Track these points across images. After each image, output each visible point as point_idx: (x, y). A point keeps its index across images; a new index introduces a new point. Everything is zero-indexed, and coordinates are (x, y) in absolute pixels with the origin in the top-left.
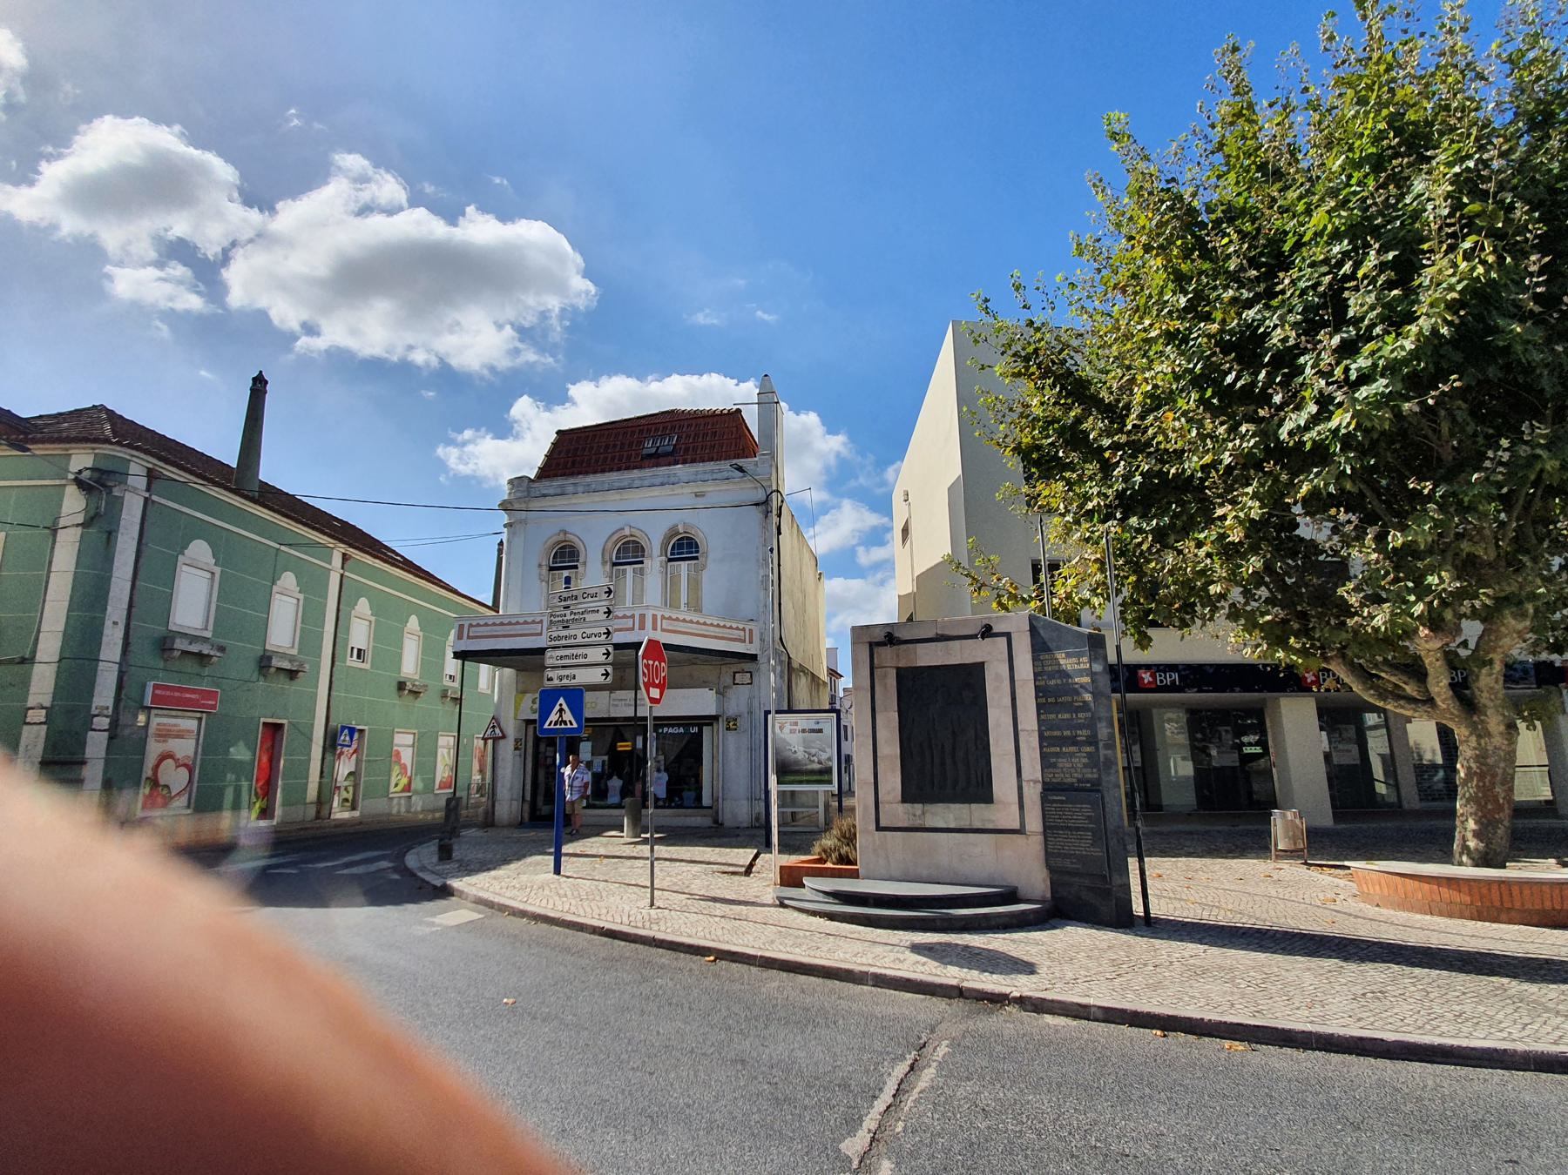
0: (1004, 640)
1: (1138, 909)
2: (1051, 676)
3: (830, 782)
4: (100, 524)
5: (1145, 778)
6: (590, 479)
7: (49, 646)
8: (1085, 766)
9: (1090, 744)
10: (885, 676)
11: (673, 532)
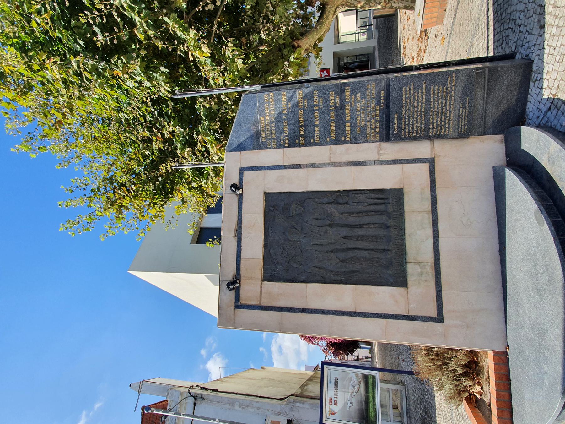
0: (246, 173)
2: (280, 131)
3: (374, 377)
8: (364, 96)
9: (343, 91)
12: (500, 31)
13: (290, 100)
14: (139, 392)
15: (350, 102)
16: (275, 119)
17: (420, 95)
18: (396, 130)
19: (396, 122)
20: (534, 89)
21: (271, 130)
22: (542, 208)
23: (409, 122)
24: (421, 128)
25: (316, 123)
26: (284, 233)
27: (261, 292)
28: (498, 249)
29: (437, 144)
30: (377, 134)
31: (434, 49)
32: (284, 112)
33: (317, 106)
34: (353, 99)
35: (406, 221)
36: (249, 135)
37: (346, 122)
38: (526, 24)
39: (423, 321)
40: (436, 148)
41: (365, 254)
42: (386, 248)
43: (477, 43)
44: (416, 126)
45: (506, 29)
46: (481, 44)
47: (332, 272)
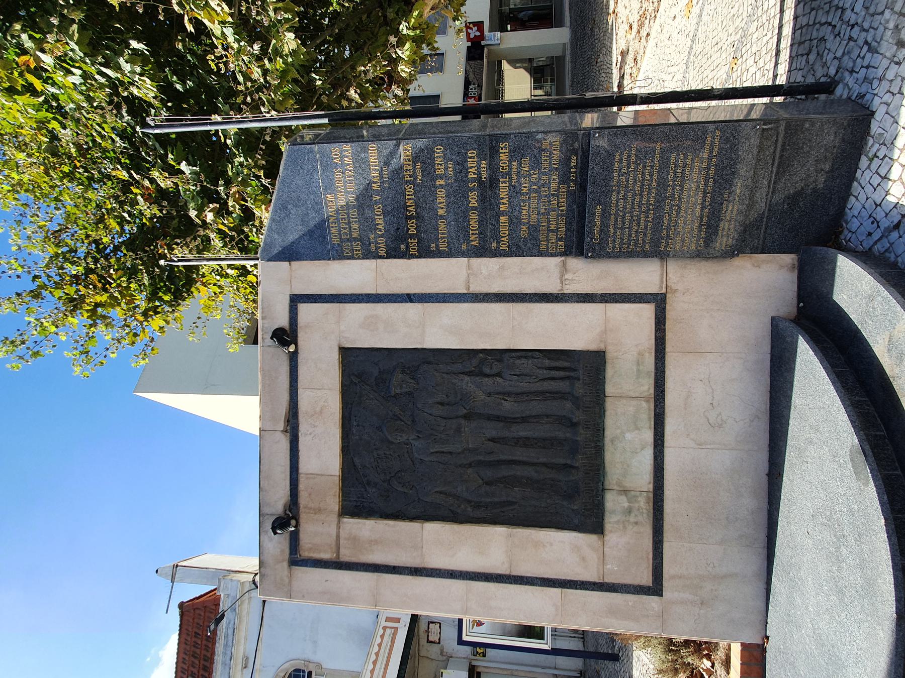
0: (303, 308)
2: (368, 224)
8: (536, 164)
10: (355, 540)
12: (808, 25)
13: (387, 163)
14: (173, 581)
15: (508, 174)
16: (357, 199)
17: (647, 171)
18: (597, 236)
19: (598, 223)
20: (868, 175)
21: (349, 222)
22: (867, 447)
23: (624, 223)
24: (645, 235)
25: (441, 212)
26: (379, 428)
27: (338, 537)
28: (767, 471)
29: (674, 268)
30: (560, 239)
31: (670, 21)
32: (375, 186)
33: (441, 178)
34: (514, 168)
35: (608, 413)
36: (305, 229)
37: (500, 214)
38: (866, 25)
39: (629, 593)
40: (670, 275)
41: (529, 472)
42: (569, 462)
43: (755, 36)
44: (637, 231)
45: (822, 25)
46: (765, 39)
47: (469, 502)
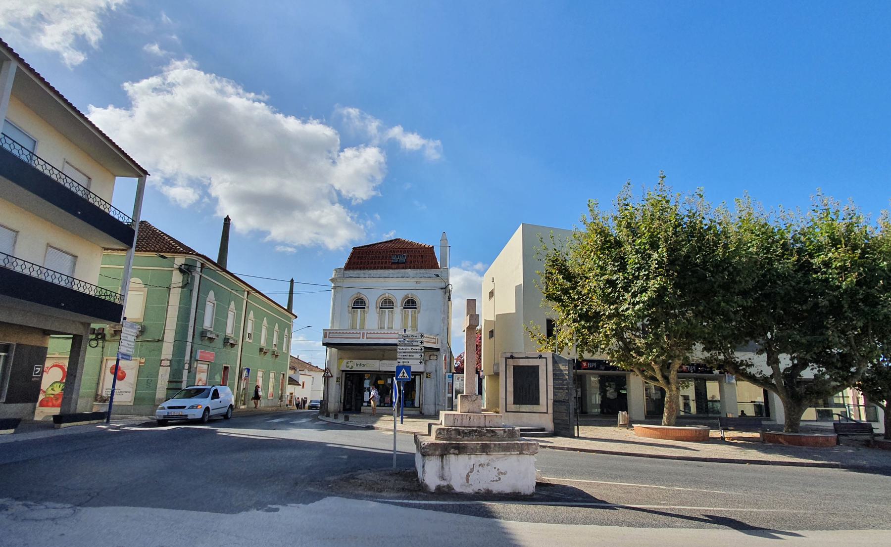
1: (576, 435)
4: (186, 285)
5: (582, 401)
6: (371, 271)
7: (170, 336)
11: (406, 297)
